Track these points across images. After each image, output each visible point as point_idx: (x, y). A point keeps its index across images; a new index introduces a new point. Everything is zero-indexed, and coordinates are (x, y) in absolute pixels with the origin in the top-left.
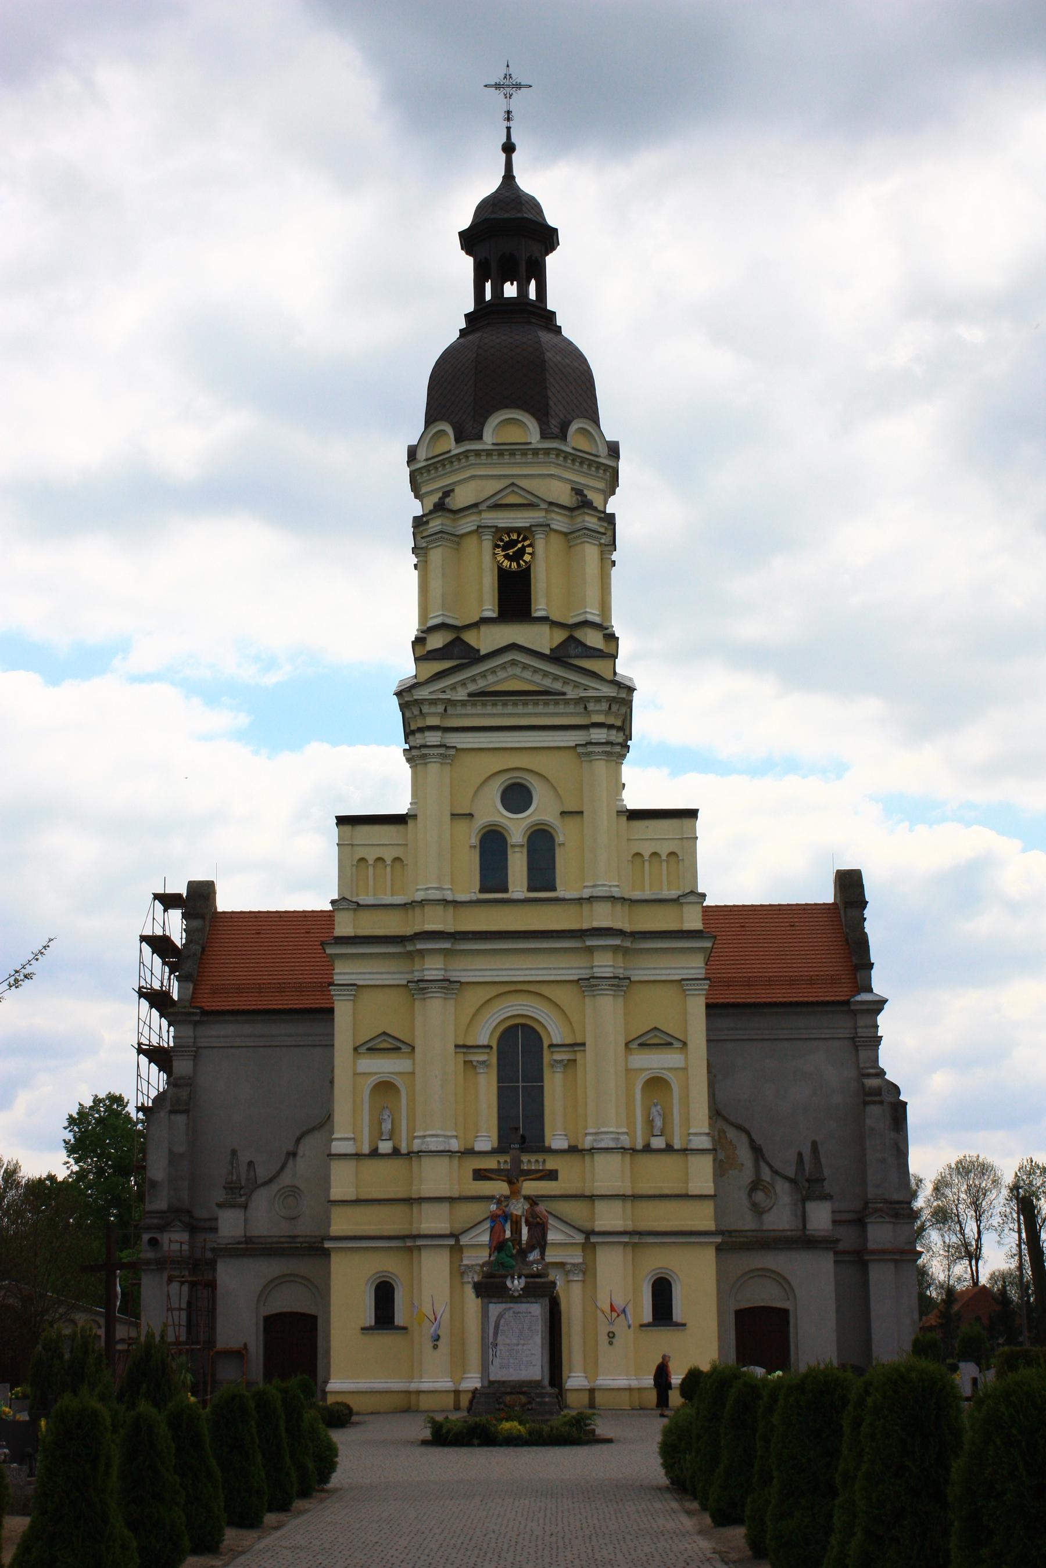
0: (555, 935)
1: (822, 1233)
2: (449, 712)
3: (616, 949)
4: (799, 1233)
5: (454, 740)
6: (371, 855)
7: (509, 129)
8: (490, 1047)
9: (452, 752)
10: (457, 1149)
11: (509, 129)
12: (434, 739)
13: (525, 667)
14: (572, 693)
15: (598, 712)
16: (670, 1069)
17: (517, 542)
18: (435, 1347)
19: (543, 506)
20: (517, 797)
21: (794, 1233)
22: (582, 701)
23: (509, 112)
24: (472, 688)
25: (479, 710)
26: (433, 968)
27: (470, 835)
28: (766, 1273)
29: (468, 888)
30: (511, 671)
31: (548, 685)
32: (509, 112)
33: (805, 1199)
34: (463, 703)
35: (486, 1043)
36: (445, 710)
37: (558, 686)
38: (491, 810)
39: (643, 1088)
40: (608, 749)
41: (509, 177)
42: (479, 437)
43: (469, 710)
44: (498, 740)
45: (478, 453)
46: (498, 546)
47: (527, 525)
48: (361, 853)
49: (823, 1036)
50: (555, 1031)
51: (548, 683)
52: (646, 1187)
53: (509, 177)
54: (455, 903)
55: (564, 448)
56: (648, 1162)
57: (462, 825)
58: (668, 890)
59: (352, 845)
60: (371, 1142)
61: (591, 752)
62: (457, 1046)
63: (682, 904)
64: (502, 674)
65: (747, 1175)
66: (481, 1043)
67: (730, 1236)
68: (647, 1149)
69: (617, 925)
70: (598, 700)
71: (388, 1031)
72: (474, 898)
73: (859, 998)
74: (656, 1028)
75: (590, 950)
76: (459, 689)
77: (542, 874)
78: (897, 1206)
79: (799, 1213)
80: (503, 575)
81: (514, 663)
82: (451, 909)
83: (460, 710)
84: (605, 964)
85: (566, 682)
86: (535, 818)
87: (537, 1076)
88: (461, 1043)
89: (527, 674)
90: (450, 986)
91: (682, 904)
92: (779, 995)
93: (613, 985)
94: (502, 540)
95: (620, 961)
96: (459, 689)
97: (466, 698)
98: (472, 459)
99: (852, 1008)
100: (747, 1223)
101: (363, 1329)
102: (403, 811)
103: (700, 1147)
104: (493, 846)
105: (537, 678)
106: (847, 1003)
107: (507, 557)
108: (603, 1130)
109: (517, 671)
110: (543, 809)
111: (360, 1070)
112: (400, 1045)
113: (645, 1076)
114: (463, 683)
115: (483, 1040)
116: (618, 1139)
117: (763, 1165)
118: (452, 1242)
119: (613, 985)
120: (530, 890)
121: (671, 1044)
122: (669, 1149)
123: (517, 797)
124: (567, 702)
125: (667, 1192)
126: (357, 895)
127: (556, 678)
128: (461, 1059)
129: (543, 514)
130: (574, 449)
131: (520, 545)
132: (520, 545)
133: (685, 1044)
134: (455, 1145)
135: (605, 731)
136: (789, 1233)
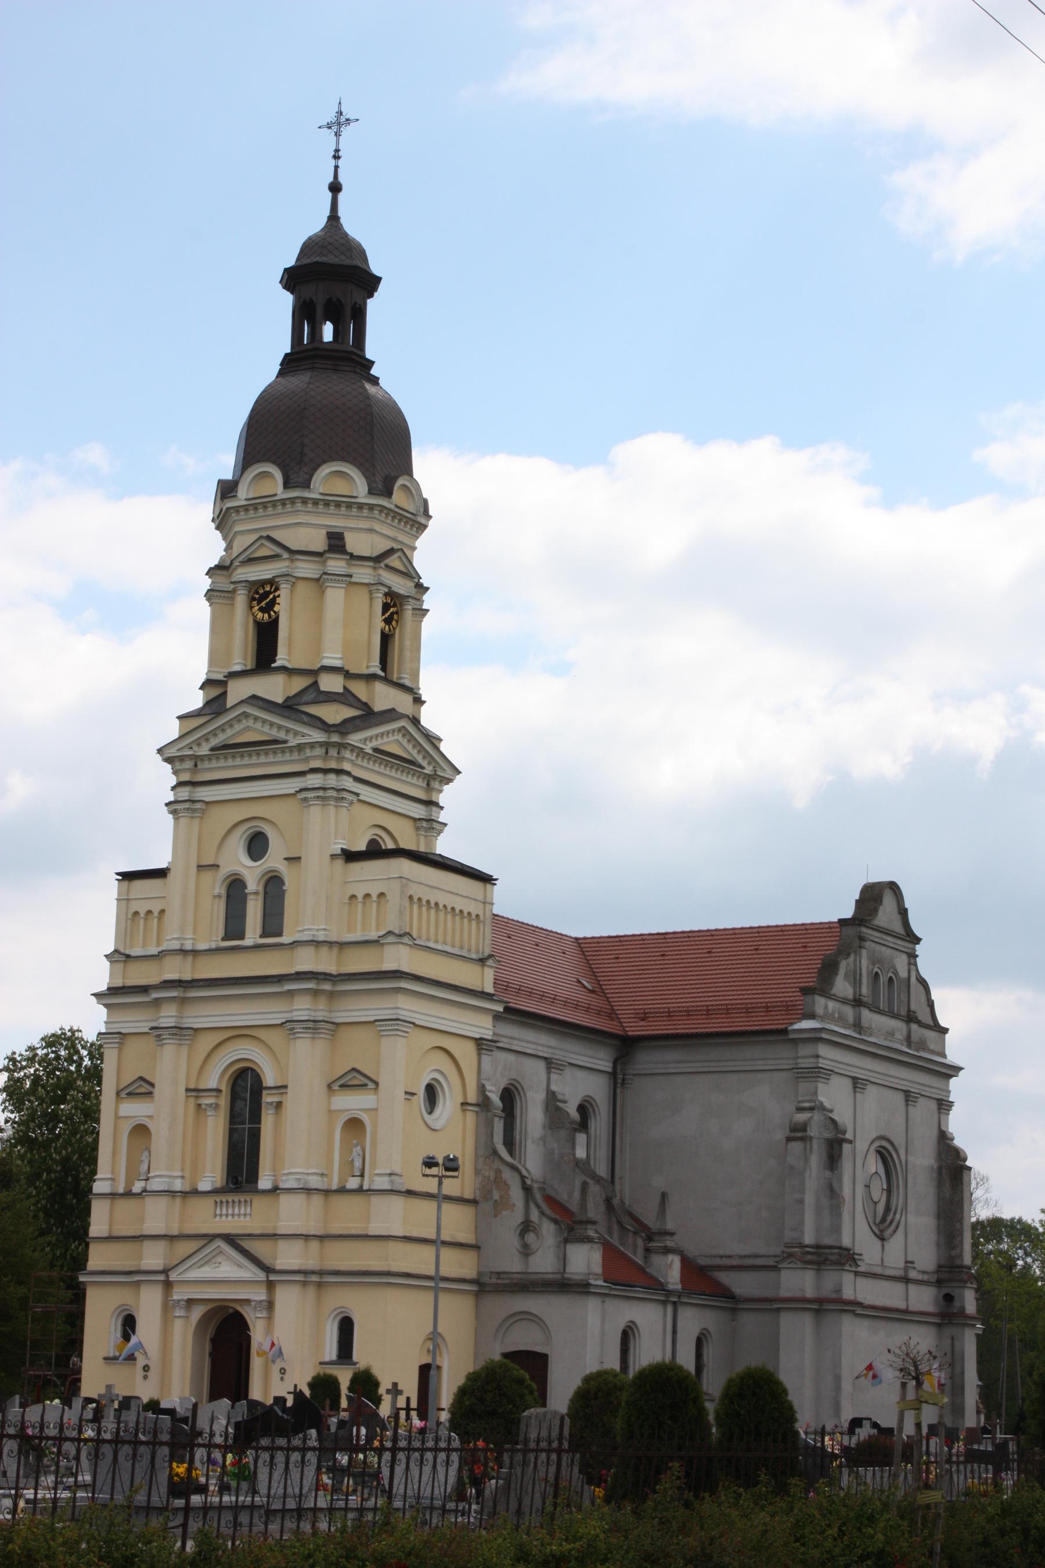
0: (219, 982)
1: (577, 1277)
2: (199, 766)
3: (315, 993)
4: (559, 1276)
5: (204, 794)
6: (142, 908)
7: (336, 167)
8: (218, 1091)
9: (198, 806)
10: (179, 1189)
11: (336, 167)
12: (316, 781)
13: (256, 718)
14: (293, 742)
15: (315, 757)
16: (359, 1110)
17: (270, 593)
18: (145, 1377)
19: (286, 555)
20: (257, 845)
21: (555, 1276)
22: (300, 748)
23: (337, 151)
24: (214, 742)
25: (222, 763)
26: (168, 1016)
27: (215, 885)
28: (527, 1316)
29: (212, 935)
30: (245, 723)
31: (275, 734)
32: (337, 151)
33: (566, 1241)
34: (209, 758)
35: (214, 1087)
36: (196, 765)
37: (282, 735)
38: (237, 859)
39: (343, 1127)
40: (321, 793)
41: (334, 217)
42: (306, 485)
43: (214, 764)
44: (259, 788)
45: (305, 501)
46: (253, 599)
47: (270, 576)
48: (135, 906)
49: (767, 1068)
50: (269, 1079)
51: (275, 734)
52: (336, 1228)
53: (334, 217)
54: (195, 953)
55: (307, 495)
56: (342, 1203)
57: (207, 876)
58: (144, 946)
59: (128, 900)
60: (340, 1180)
61: (343, 798)
62: (187, 1090)
63: (383, 944)
64: (238, 727)
65: (518, 1217)
66: (210, 1087)
67: (499, 1278)
68: (342, 1190)
69: (321, 968)
70: (312, 745)
71: (358, 1067)
72: (214, 946)
73: (796, 1026)
74: (354, 1069)
75: (157, 1003)
76: (204, 744)
77: (272, 924)
78: (827, 1251)
79: (561, 1255)
80: (259, 626)
81: (246, 715)
82: (190, 958)
83: (206, 765)
84: (168, 1016)
85: (288, 730)
86: (266, 866)
87: (256, 1116)
88: (192, 1086)
89: (258, 725)
90: (179, 1031)
91: (383, 944)
92: (681, 1027)
93: (306, 1028)
94: (257, 592)
95: (322, 1003)
96: (204, 744)
97: (208, 753)
98: (299, 506)
99: (791, 1036)
100: (512, 1264)
101: (105, 1359)
102: (164, 866)
103: (381, 1188)
104: (235, 887)
105: (266, 728)
106: (784, 1032)
107: (261, 610)
108: (292, 1170)
109: (250, 722)
110: (274, 860)
111: (122, 1113)
112: (366, 1081)
113: (346, 1117)
114: (206, 738)
115: (213, 1084)
116: (299, 1180)
117: (532, 1206)
118: (162, 1278)
119: (306, 1028)
120: (264, 935)
121: (366, 1085)
122: (360, 1190)
123: (257, 845)
124: (291, 749)
125: (353, 1232)
126: (132, 947)
127: (280, 727)
128: (192, 1101)
129: (287, 563)
130: (321, 494)
131: (271, 596)
132: (271, 596)
133: (377, 1084)
134: (178, 1185)
135: (320, 776)
136: (551, 1276)
